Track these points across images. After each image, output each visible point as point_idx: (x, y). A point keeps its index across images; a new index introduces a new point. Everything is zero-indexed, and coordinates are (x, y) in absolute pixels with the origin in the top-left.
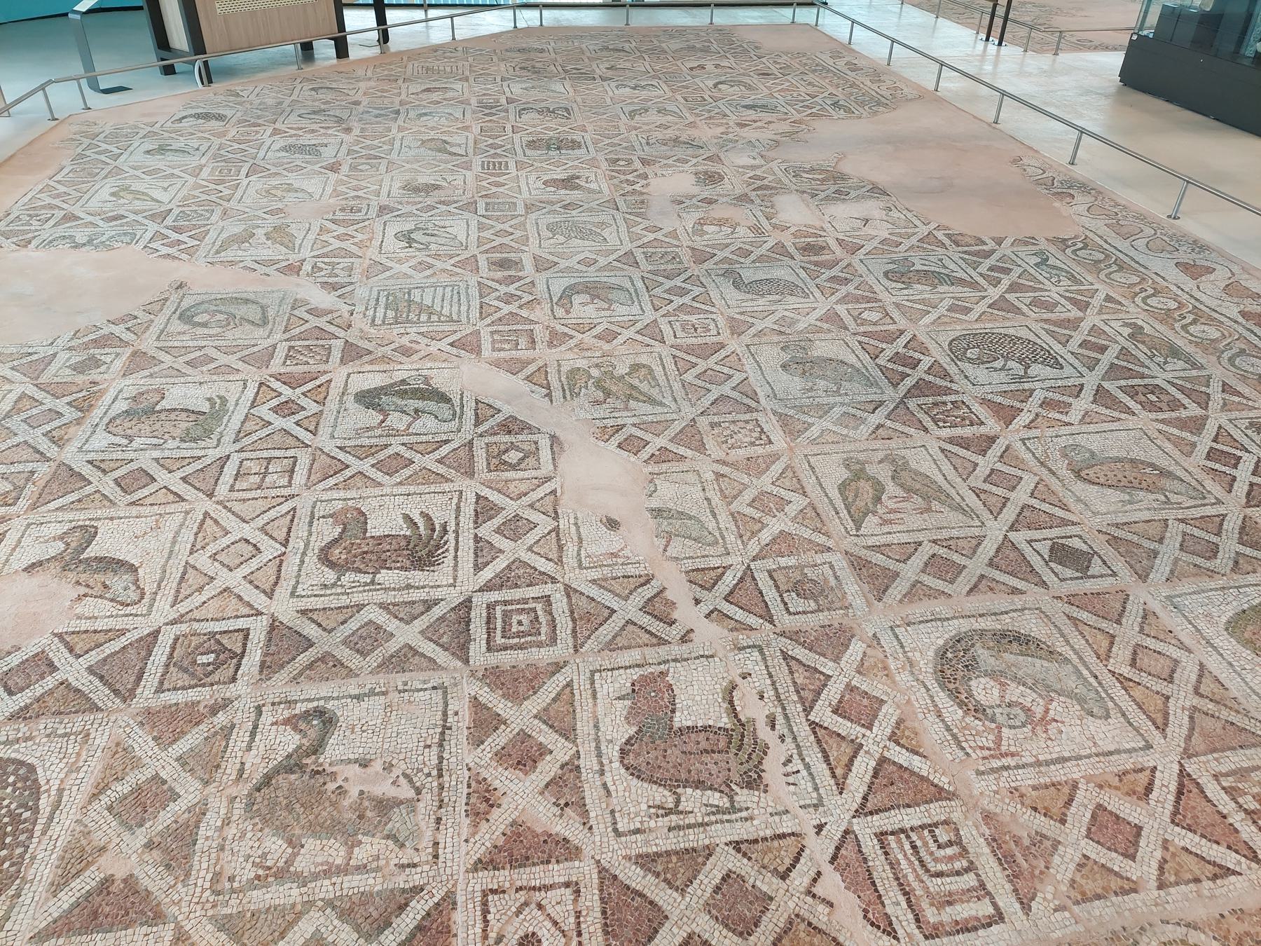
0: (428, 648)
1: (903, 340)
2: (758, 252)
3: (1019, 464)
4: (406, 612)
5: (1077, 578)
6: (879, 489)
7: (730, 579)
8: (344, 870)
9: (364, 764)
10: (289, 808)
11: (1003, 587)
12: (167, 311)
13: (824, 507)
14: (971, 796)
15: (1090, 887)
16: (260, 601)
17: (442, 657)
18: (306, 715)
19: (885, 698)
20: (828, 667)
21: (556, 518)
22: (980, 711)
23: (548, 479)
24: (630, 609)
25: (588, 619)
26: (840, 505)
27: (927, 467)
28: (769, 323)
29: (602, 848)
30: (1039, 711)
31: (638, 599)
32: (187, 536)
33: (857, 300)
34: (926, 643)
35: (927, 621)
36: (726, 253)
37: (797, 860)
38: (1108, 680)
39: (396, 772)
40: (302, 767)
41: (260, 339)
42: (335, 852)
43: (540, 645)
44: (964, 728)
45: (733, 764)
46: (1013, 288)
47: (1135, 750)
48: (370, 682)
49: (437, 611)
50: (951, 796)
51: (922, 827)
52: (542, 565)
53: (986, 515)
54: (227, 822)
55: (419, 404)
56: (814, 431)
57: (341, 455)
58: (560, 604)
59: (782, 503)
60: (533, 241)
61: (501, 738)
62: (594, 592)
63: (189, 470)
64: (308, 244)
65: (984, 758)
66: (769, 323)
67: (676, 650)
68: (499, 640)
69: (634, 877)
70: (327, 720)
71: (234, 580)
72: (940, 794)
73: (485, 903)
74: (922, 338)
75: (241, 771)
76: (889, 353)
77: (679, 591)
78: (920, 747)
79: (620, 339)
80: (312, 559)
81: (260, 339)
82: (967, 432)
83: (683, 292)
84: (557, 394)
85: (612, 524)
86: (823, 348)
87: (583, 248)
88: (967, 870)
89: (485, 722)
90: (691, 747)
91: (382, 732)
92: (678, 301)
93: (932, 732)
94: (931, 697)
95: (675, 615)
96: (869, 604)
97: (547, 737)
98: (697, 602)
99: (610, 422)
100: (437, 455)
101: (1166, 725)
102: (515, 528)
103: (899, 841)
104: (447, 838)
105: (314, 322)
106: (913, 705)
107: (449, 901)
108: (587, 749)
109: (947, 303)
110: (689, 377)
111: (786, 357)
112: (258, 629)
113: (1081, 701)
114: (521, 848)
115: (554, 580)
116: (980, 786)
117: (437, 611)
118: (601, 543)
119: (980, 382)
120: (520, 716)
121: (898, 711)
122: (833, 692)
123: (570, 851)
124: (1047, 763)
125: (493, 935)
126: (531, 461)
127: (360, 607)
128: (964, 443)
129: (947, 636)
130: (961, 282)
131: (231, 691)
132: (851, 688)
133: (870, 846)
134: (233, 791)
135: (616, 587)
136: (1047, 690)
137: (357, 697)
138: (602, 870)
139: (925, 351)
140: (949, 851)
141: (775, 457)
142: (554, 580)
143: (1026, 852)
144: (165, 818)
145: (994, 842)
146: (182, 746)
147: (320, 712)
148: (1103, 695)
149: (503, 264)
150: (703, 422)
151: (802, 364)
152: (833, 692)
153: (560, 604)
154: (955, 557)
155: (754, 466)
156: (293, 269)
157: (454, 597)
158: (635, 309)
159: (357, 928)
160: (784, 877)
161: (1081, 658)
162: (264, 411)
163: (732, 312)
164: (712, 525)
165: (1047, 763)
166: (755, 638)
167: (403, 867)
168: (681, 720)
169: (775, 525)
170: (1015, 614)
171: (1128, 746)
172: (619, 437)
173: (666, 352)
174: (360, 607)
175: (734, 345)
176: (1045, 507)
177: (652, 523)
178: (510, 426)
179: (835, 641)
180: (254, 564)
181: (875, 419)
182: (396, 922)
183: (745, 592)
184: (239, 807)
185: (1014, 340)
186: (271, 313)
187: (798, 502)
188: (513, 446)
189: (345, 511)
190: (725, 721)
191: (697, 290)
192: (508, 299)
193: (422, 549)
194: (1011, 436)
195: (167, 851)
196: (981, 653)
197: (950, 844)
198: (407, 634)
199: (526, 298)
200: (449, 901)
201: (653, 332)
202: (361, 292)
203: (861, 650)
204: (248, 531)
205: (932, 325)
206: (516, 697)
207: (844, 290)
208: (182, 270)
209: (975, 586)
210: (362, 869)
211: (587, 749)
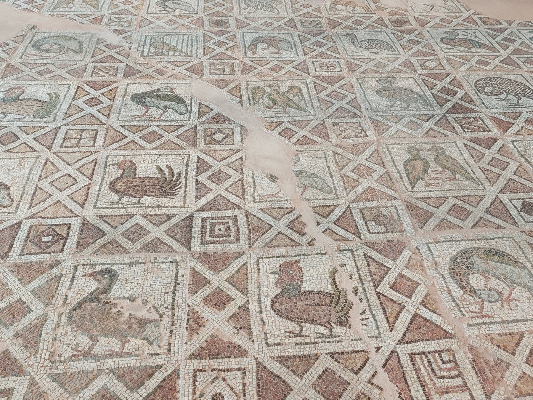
0: (169, 240)
1: (448, 80)
2: (367, 23)
3: (509, 155)
4: (157, 220)
6: (427, 166)
7: (337, 213)
8: (120, 355)
9: (132, 300)
10: (91, 320)
11: (492, 225)
12: (26, 42)
13: (394, 175)
14: (463, 337)
15: (525, 389)
16: (77, 209)
17: (176, 246)
18: (101, 272)
19: (420, 282)
20: (389, 263)
21: (242, 173)
22: (473, 292)
23: (238, 151)
24: (281, 226)
25: (257, 229)
26: (404, 174)
27: (455, 154)
28: (371, 66)
29: (258, 351)
30: (506, 294)
31: (285, 221)
32: (37, 171)
33: (424, 54)
34: (446, 253)
36: (348, 23)
37: (364, 364)
39: (149, 305)
40: (98, 300)
41: (79, 61)
42: (115, 344)
43: (230, 242)
44: (463, 301)
45: (333, 313)
46: (516, 51)
48: (136, 257)
49: (174, 221)
50: (452, 336)
51: (435, 352)
52: (233, 199)
53: (487, 183)
54: (58, 326)
55: (167, 103)
56: (392, 131)
57: (123, 130)
58: (242, 221)
59: (371, 171)
60: (236, 10)
61: (206, 291)
62: (261, 215)
63: (38, 134)
64: (106, 6)
66: (371, 66)
67: (305, 249)
68: (208, 238)
69: (276, 368)
70: (113, 276)
71: (63, 196)
72: (446, 335)
73: (195, 376)
74: (460, 79)
75: (66, 300)
76: (439, 87)
77: (309, 218)
78: (437, 309)
79: (283, 71)
80: (105, 188)
81: (79, 61)
82: (480, 135)
83: (321, 45)
84: (245, 101)
85: (273, 178)
86: (401, 82)
87: (265, 15)
88: (458, 376)
89: (198, 282)
90: (310, 302)
91: (141, 284)
92: (318, 50)
93: (445, 301)
94: (446, 283)
95: (306, 230)
96: (415, 230)
97: (232, 292)
98: (318, 224)
99: (275, 120)
100: (176, 133)
102: (218, 177)
103: (421, 359)
104: (176, 341)
105: (109, 52)
107: (176, 374)
108: (253, 299)
109: (476, 58)
110: (322, 95)
111: (379, 86)
112: (76, 224)
114: (215, 349)
115: (239, 207)
116: (470, 332)
117: (174, 221)
118: (266, 188)
119: (494, 106)
120: (218, 280)
122: (391, 277)
123: (241, 352)
124: (508, 322)
125: (198, 393)
126: (229, 140)
127: (132, 216)
128: (478, 141)
129: (458, 250)
130: (485, 46)
131: (61, 256)
132: (401, 276)
133: (405, 360)
134: (62, 310)
135: (274, 214)
136: (512, 283)
137: (130, 264)
138: (258, 363)
139: (460, 87)
140: (449, 366)
141: (369, 144)
142: (239, 207)
143: (491, 369)
144: (25, 322)
145: (474, 363)
146: (34, 285)
147: (109, 271)
149: (218, 23)
150: (329, 122)
151: (388, 91)
152: (391, 277)
153: (242, 221)
154: (467, 206)
155: (356, 150)
156: (97, 21)
157: (184, 213)
158: (293, 54)
159: (126, 385)
160: (357, 373)
162: (80, 103)
163: (350, 58)
164: (330, 182)
165: (508, 322)
166: (349, 245)
167: (152, 355)
168: (305, 287)
169: (365, 184)
170: (498, 240)
172: (280, 129)
173: (309, 79)
174: (132, 216)
175: (350, 78)
176: (522, 181)
177: (296, 179)
178: (218, 119)
179: (395, 249)
180: (74, 188)
181: (427, 125)
182: (147, 383)
183: (346, 220)
184: (64, 319)
185: (513, 83)
186: (84, 46)
187: (380, 171)
188: (219, 131)
189: (124, 162)
190: (330, 289)
191: (330, 44)
192: (220, 44)
193: (166, 185)
194: (506, 139)
195: (25, 339)
196: (477, 261)
197: (450, 361)
198: (158, 232)
199: (231, 44)
200: (176, 374)
201: (302, 67)
202: (136, 36)
203: (409, 255)
204: (70, 170)
205: (465, 70)
206: (216, 269)
207: (416, 48)
208: (34, 18)
209: (477, 223)
210: (129, 354)
211: (253, 299)
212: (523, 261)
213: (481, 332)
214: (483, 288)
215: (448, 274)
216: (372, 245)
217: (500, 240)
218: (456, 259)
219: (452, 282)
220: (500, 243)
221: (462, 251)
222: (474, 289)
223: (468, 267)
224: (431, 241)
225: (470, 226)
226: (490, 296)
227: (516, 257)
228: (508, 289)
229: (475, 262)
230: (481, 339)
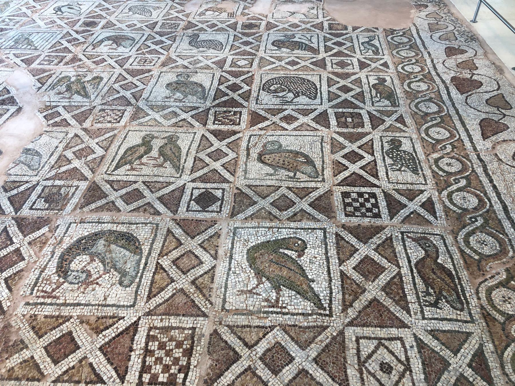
5: (196, 211)
94: (50, 261)
96: (75, 209)
113: (123, 274)
129: (93, 231)
148: (139, 275)
161: (149, 254)
218: (82, 240)
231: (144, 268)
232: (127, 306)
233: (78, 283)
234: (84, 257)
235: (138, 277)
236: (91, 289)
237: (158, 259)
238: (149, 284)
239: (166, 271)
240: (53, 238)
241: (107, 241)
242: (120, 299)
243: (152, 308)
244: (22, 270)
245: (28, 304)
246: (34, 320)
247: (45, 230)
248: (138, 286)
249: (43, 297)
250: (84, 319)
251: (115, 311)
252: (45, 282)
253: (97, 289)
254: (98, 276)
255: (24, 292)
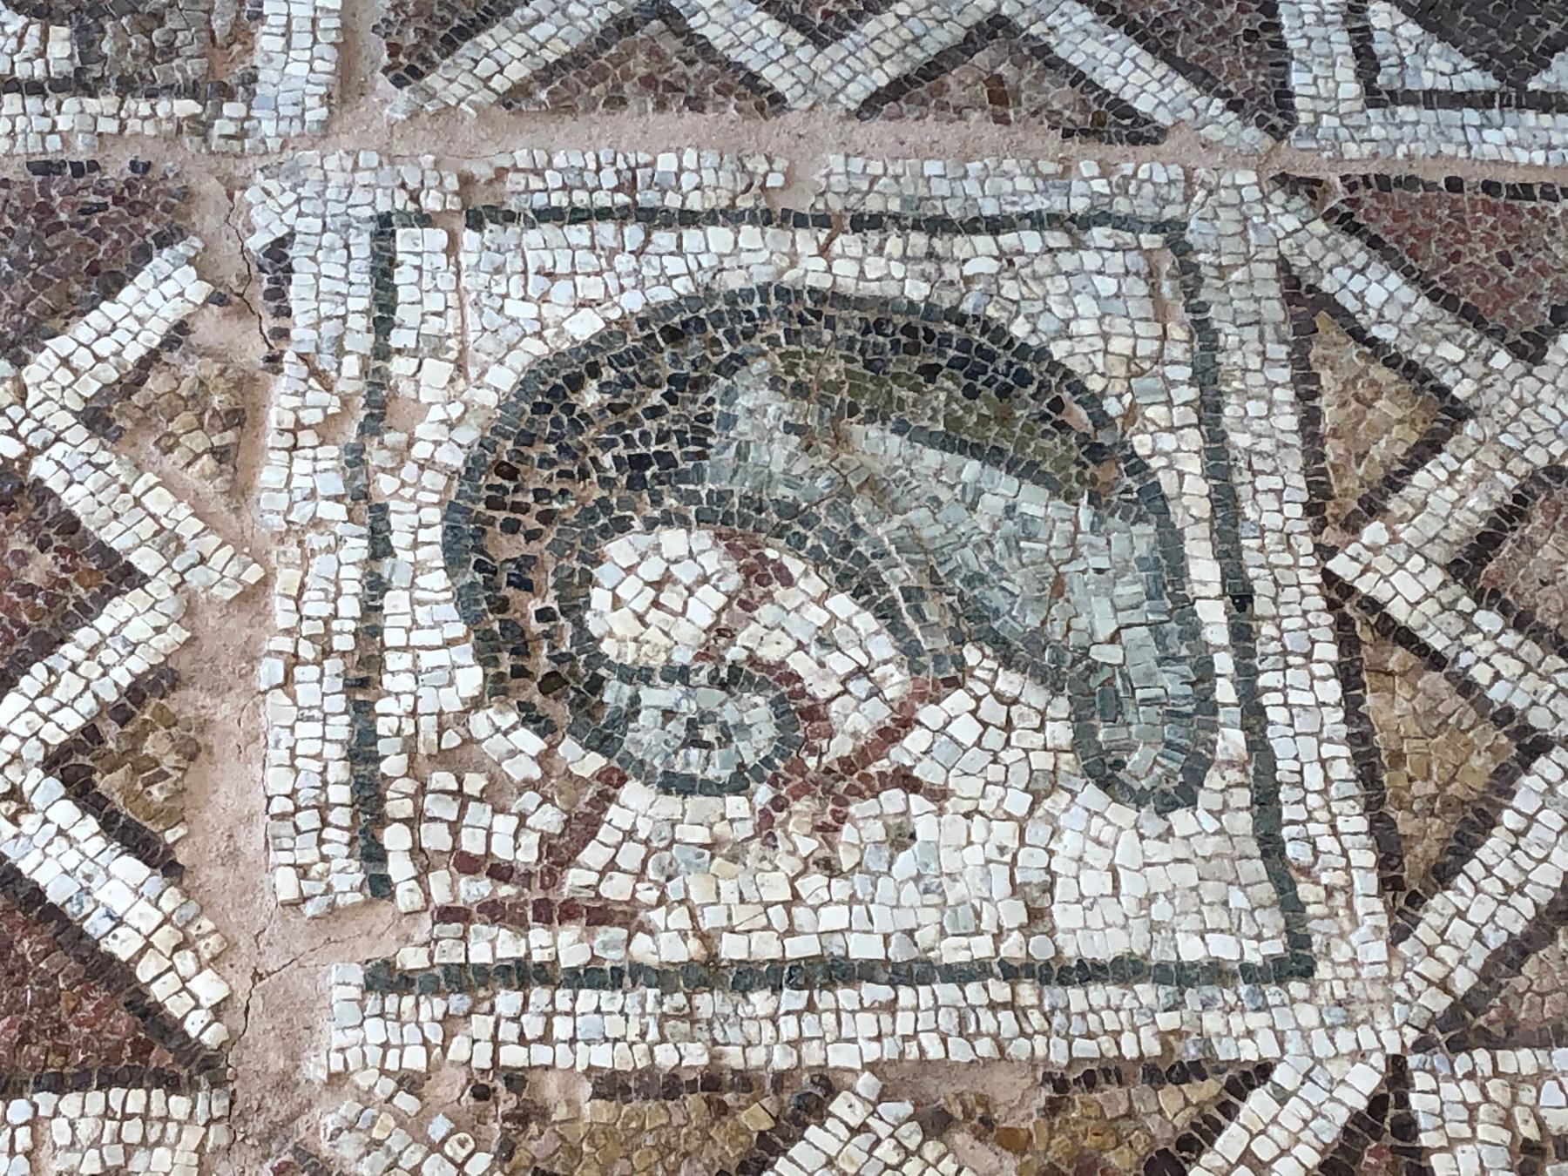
5: (1457, 100)
11: (1059, 96)
14: (285, 1083)
19: (146, 561)
34: (511, 312)
35: (579, 216)
38: (1296, 616)
44: (443, 758)
47: (1216, 972)
65: (447, 914)
78: (174, 817)
94: (376, 586)
96: (345, 89)
101: (1442, 876)
106: (264, 614)
113: (1093, 696)
121: (177, 634)
124: (747, 977)
129: (633, 302)
148: (1225, 692)
161: (1225, 503)
165: (747, 977)
170: (1031, 240)
171: (1191, 951)
203: (172, 312)
209: (933, 70)
212: (1167, 442)
213: (459, 1049)
214: (682, 657)
215: (433, 515)
216: (1373, 211)
217: (1057, 239)
218: (576, 383)
219: (436, 581)
220: (1043, 266)
221: (667, 309)
222: (598, 658)
223: (640, 462)
224: (431, 203)
225: (857, 92)
226: (708, 734)
227: (1112, 407)
228: (896, 682)
229: (729, 421)
230: (424, 1117)
231: (1242, 635)
232: (1248, 972)
233: (739, 784)
234: (673, 540)
235: (1230, 715)
236: (876, 831)
237: (1325, 552)
238: (1343, 769)
239: (1436, 661)
240: (292, 368)
241: (800, 390)
242: (1160, 910)
243: (1463, 981)
244: (159, 682)
245: (385, 979)
246: (521, 1118)
247: (161, 293)
248: (1266, 800)
249: (493, 911)
250: (943, 1093)
251: (1167, 1021)
252: (443, 779)
253: (925, 827)
254: (879, 713)
255: (303, 871)
